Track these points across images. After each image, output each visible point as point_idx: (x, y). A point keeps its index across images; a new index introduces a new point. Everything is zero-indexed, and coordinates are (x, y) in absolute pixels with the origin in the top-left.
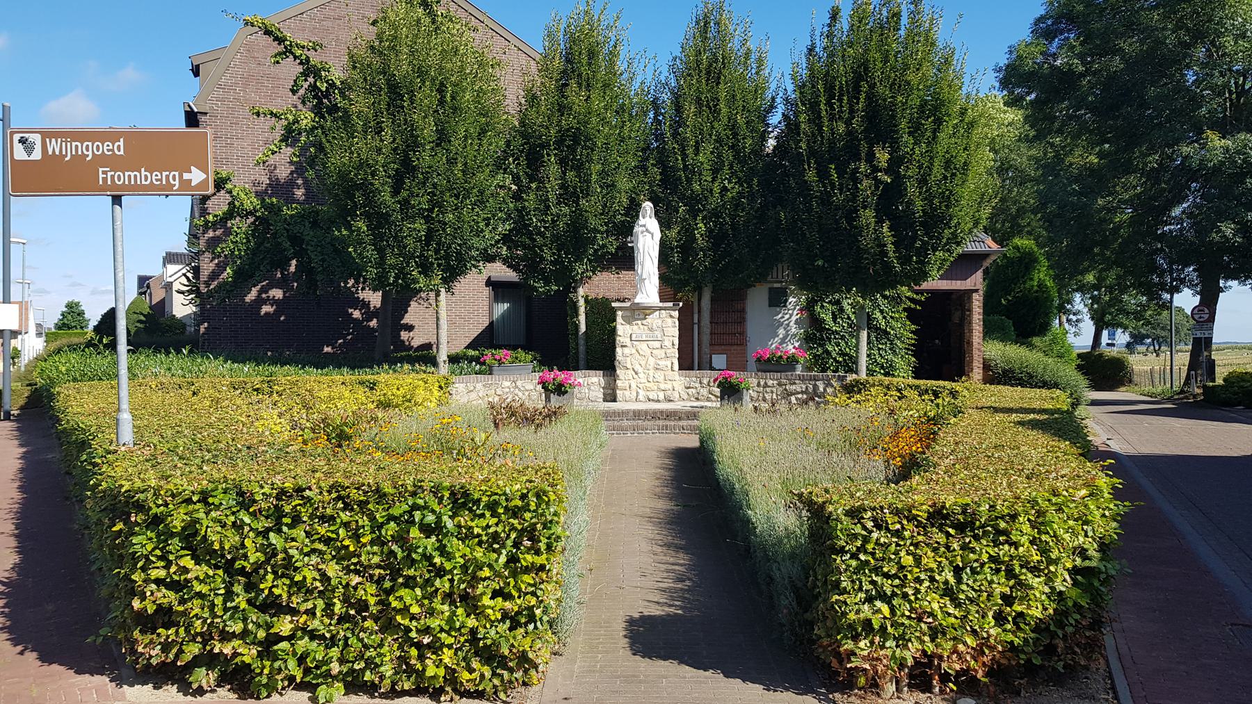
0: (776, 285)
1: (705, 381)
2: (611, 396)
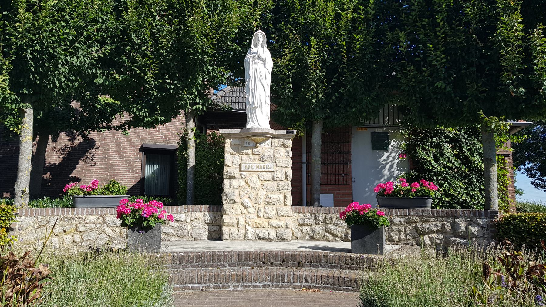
0: (378, 130)
1: (321, 217)
2: (216, 234)
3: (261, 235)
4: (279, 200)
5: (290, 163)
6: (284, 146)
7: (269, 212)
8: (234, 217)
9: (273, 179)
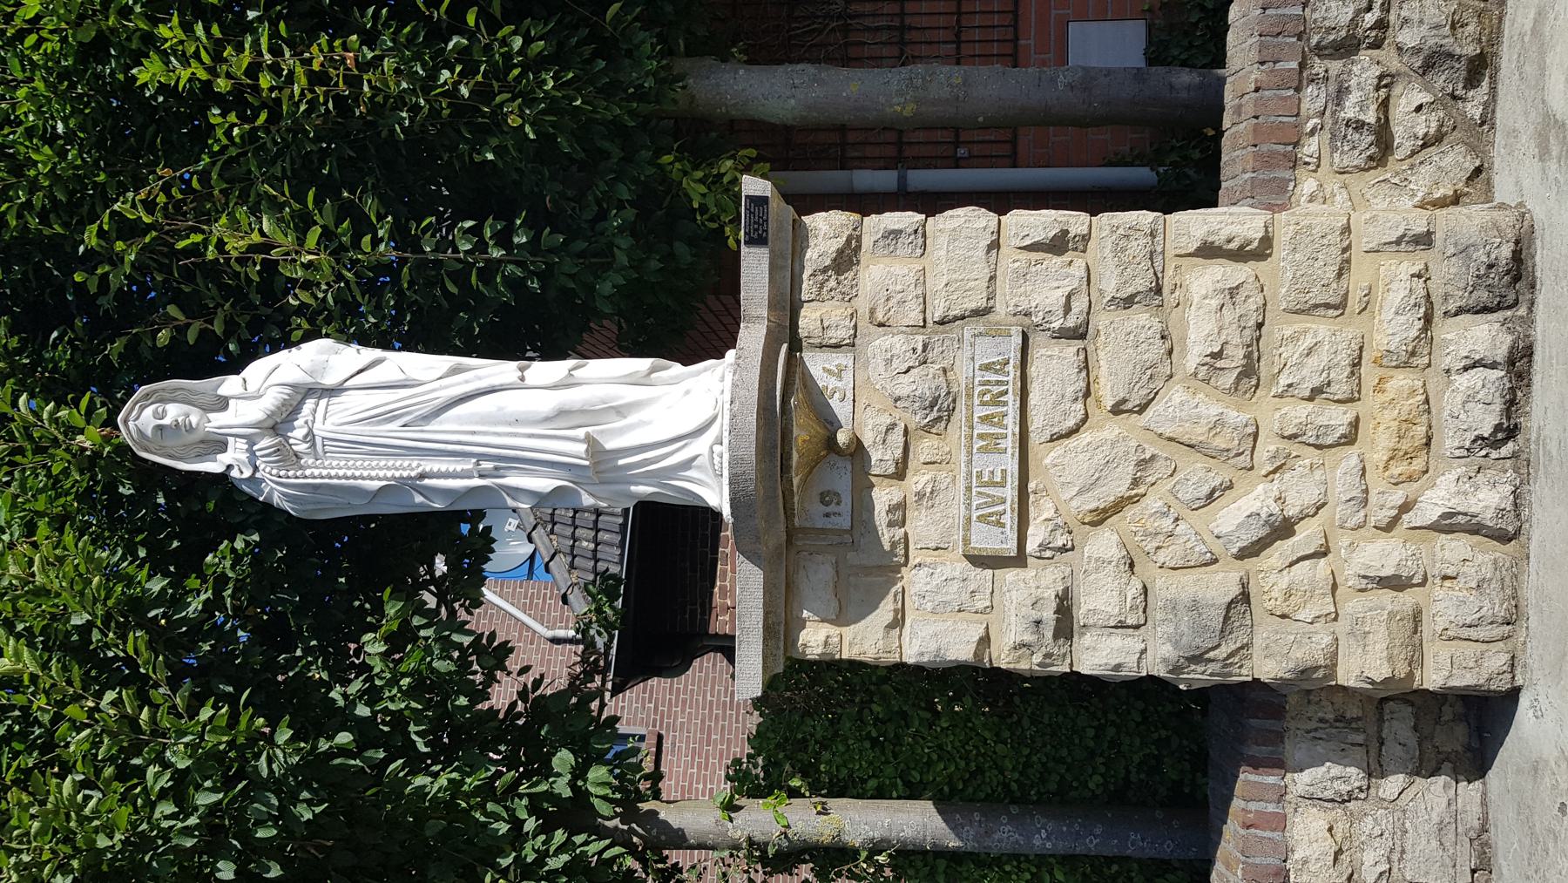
3: (1487, 423)
4: (1233, 292)
5: (970, 221)
6: (846, 259)
7: (1312, 362)
8: (1353, 605)
9: (1078, 334)
